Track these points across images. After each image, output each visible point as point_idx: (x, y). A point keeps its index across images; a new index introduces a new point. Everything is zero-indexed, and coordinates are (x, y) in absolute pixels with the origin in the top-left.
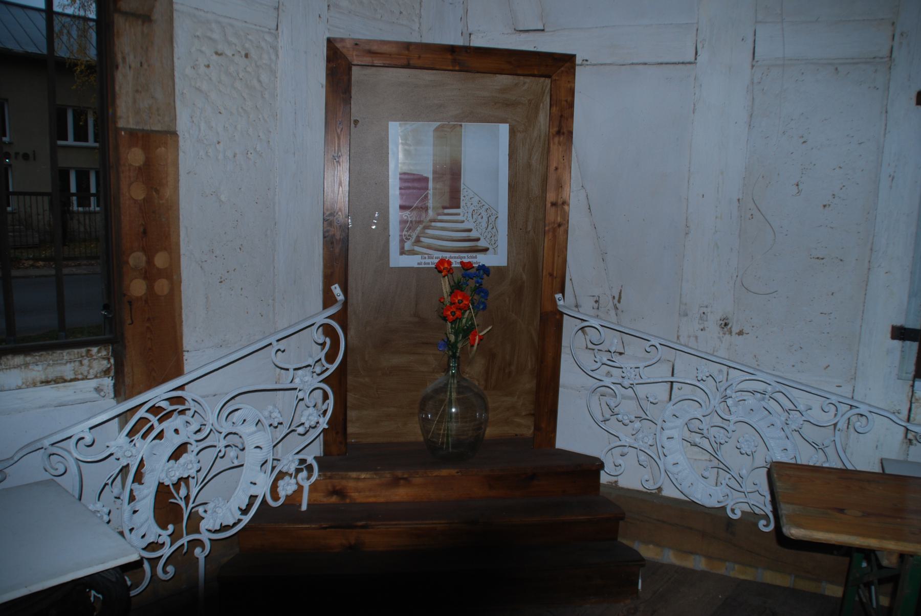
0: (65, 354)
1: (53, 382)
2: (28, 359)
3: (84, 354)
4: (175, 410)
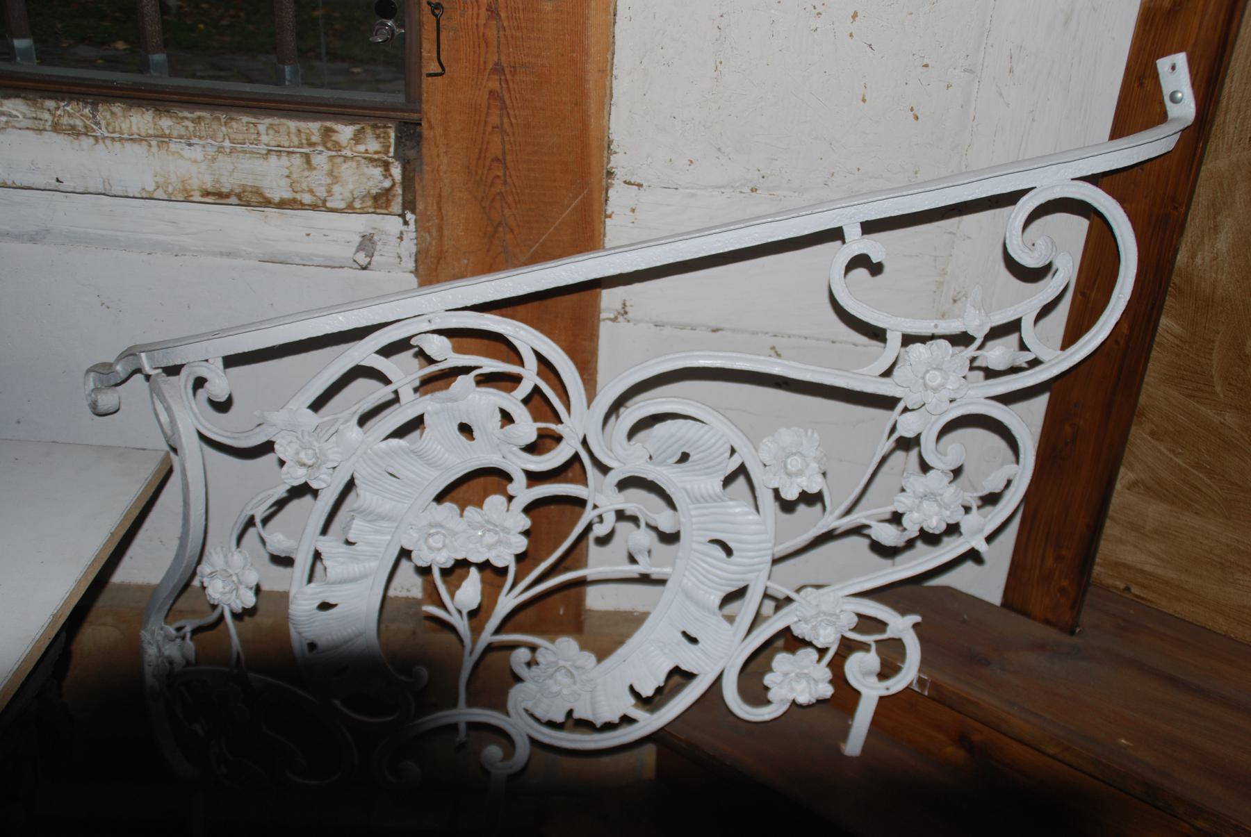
0: (262, 128)
1: (233, 200)
2: (166, 123)
3: (315, 138)
4: (466, 370)
